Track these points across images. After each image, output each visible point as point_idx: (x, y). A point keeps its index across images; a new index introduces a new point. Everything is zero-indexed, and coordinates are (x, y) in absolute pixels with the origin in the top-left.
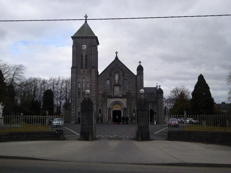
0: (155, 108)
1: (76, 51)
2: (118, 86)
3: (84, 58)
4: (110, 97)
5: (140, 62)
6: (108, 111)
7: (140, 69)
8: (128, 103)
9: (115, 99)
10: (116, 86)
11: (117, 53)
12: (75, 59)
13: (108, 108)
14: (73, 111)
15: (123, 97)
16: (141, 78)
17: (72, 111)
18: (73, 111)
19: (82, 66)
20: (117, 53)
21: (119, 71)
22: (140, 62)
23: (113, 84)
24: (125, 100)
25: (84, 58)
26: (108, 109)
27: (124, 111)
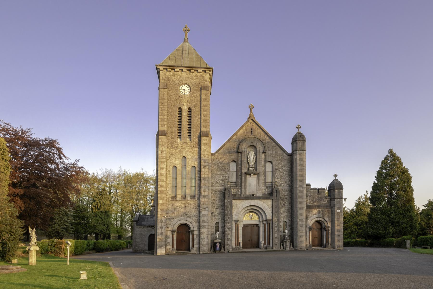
0: (327, 219)
1: (166, 99)
2: (255, 174)
3: (185, 114)
4: (237, 197)
5: (299, 127)
6: (234, 226)
7: (298, 140)
8: (275, 209)
9: (250, 201)
10: (250, 174)
11: (251, 107)
12: (166, 114)
13: (234, 219)
14: (161, 227)
15: (264, 198)
16: (302, 159)
17: (158, 227)
18: (161, 227)
19: (66, 265)
20: (251, 107)
21: (257, 144)
22: (299, 127)
23: (244, 170)
24: (269, 202)
25: (185, 114)
26: (234, 223)
27: (265, 225)
